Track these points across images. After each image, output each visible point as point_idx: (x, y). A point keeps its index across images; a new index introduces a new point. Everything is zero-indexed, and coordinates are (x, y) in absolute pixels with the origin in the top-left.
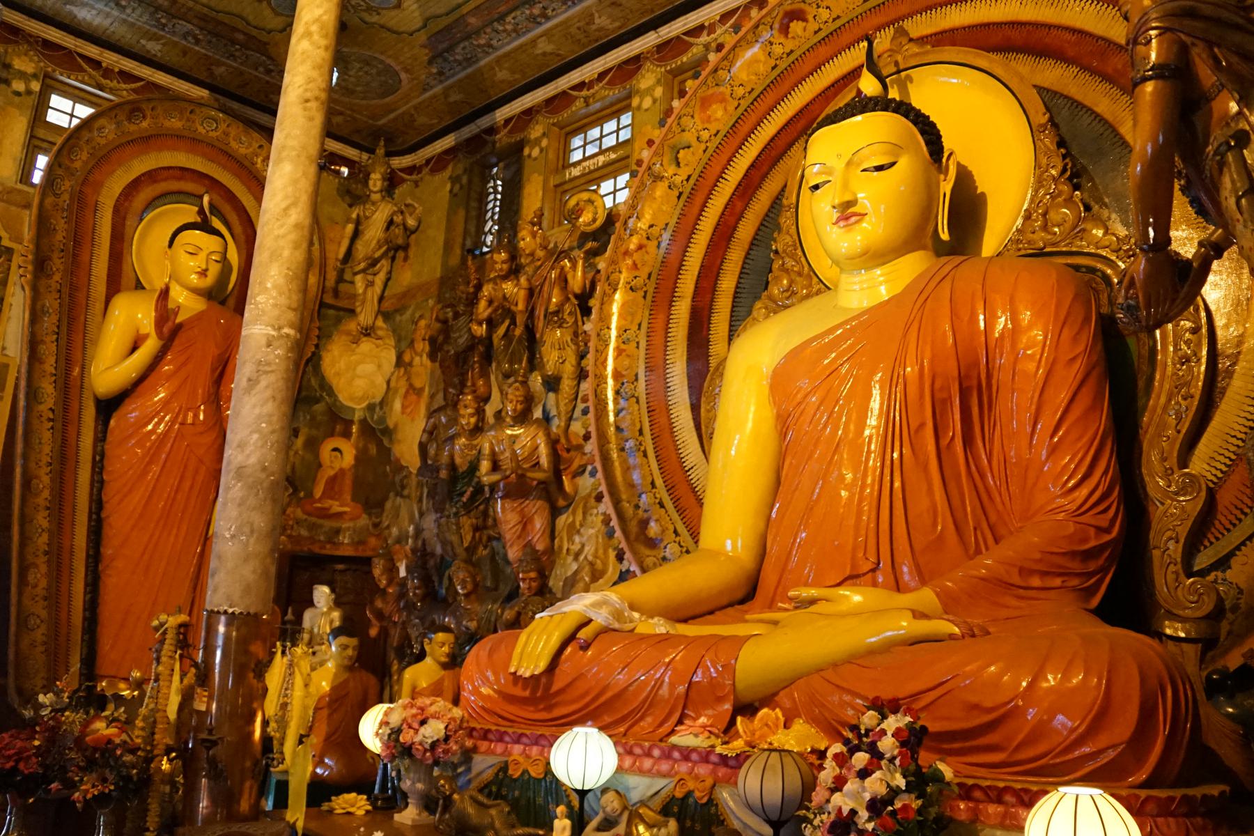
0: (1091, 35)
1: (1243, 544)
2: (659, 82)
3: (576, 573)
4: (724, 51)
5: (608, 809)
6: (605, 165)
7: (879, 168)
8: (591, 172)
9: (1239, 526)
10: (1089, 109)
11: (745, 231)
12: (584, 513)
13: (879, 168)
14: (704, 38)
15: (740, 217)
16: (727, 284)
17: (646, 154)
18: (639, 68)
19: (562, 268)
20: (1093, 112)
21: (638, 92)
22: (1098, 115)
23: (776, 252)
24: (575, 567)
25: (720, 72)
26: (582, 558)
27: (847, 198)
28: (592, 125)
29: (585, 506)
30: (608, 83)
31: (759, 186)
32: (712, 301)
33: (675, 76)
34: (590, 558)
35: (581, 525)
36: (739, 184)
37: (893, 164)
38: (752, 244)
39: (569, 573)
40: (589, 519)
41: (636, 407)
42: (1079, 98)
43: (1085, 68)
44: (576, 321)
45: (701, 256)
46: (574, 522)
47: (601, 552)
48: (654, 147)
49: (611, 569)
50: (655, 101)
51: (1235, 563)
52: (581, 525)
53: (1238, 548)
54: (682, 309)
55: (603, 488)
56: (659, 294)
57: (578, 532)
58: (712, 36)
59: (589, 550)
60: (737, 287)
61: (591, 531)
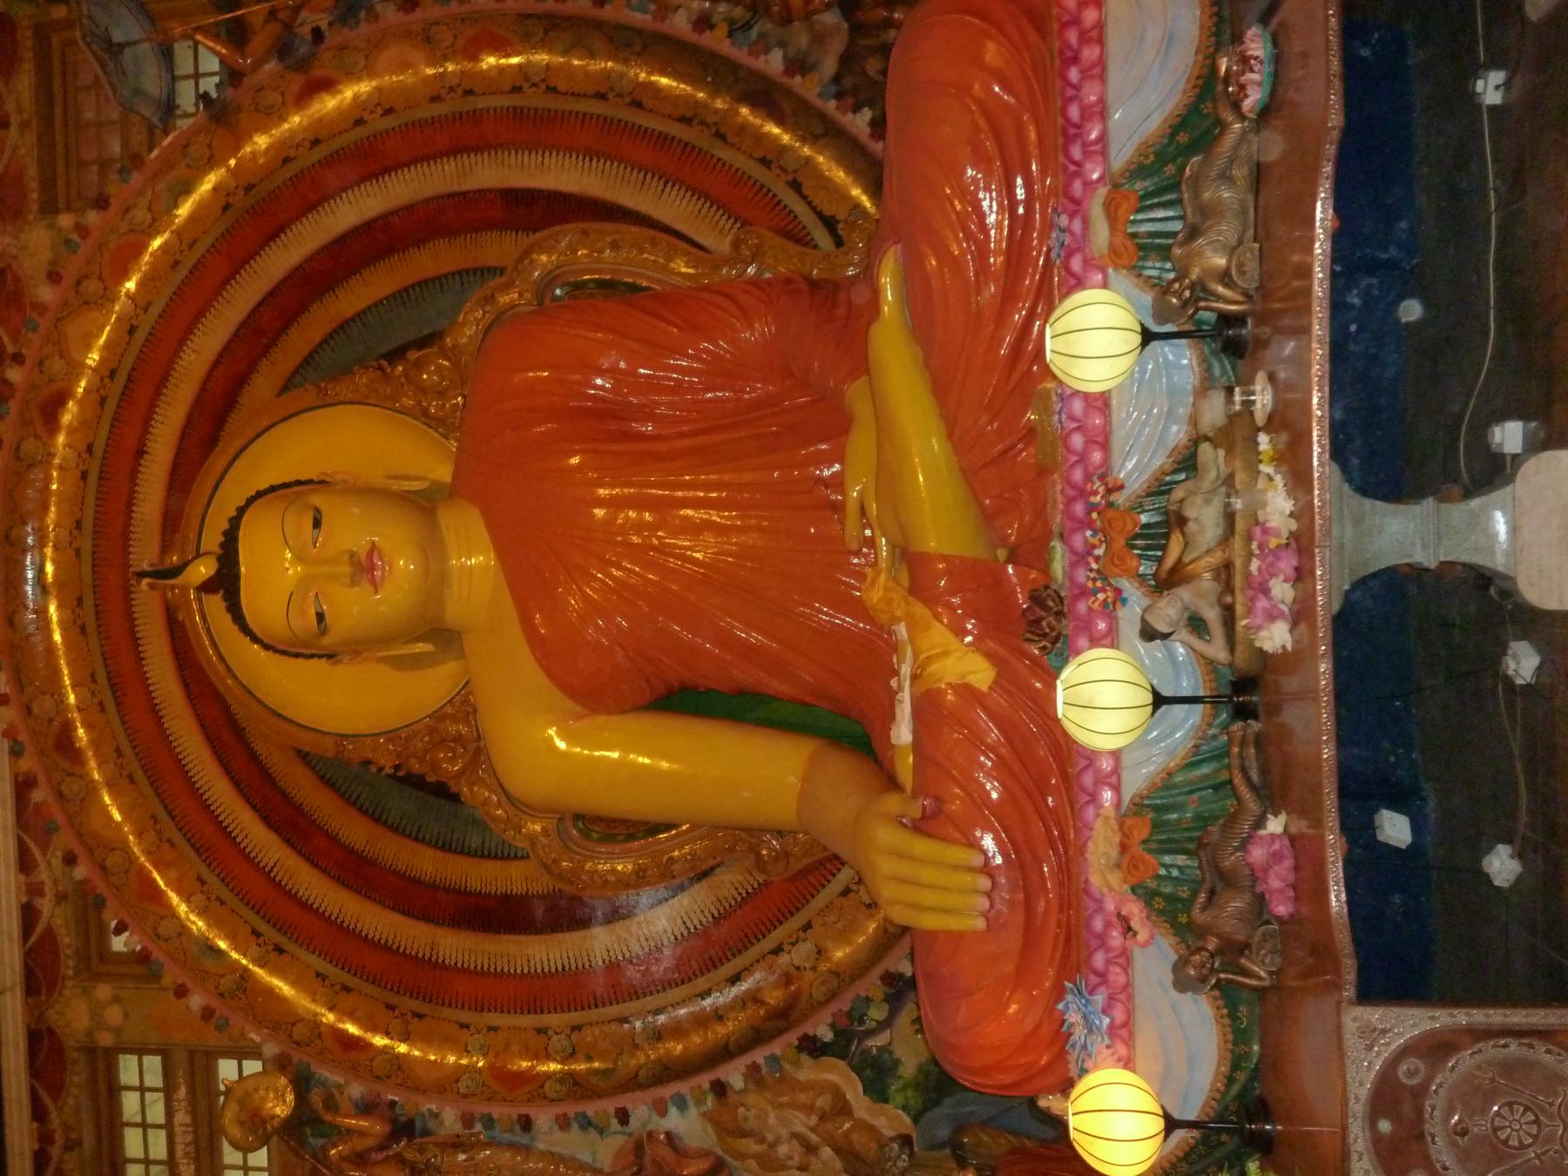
0: (229, 342)
1: (809, 203)
2: (86, 992)
3: (837, 1150)
4: (79, 850)
5: (1190, 388)
6: (193, 1111)
7: (317, 524)
8: (196, 1142)
9: (781, 196)
10: (315, 351)
11: (356, 831)
12: (744, 1134)
13: (317, 524)
14: (45, 905)
15: (334, 839)
16: (426, 863)
17: (196, 1001)
18: (50, 1031)
19: (342, 1159)
20: (320, 344)
21: (90, 1034)
22: (325, 341)
23: (397, 768)
24: (827, 1152)
25: (109, 863)
26: (814, 1138)
27: (346, 558)
28: (116, 1142)
29: (730, 1133)
30: (55, 1098)
31: (299, 810)
32: (448, 890)
33: (88, 968)
34: (814, 1120)
35: (763, 1140)
36: (287, 841)
37: (317, 510)
38: (378, 821)
39: (838, 1165)
40: (753, 1123)
41: (587, 1031)
42: (297, 359)
43: (266, 350)
44: (436, 1144)
45: (378, 909)
46: (755, 1156)
47: (803, 1098)
48: (189, 985)
49: (829, 1077)
50: (116, 1000)
51: (828, 210)
52: (763, 1140)
53: (814, 209)
54: (454, 945)
55: (704, 1080)
56: (412, 989)
57: (773, 1146)
58: (47, 889)
59: (801, 1123)
60: (436, 846)
61: (772, 1120)
